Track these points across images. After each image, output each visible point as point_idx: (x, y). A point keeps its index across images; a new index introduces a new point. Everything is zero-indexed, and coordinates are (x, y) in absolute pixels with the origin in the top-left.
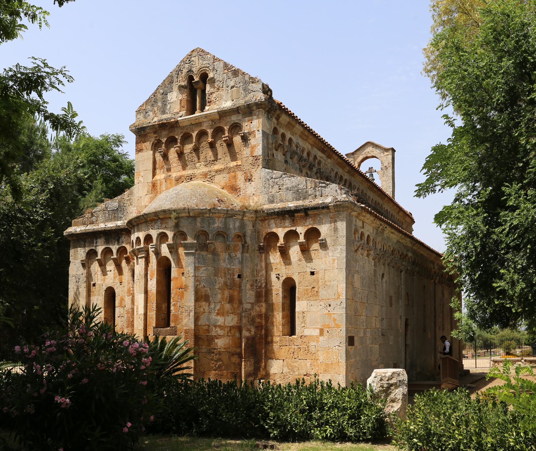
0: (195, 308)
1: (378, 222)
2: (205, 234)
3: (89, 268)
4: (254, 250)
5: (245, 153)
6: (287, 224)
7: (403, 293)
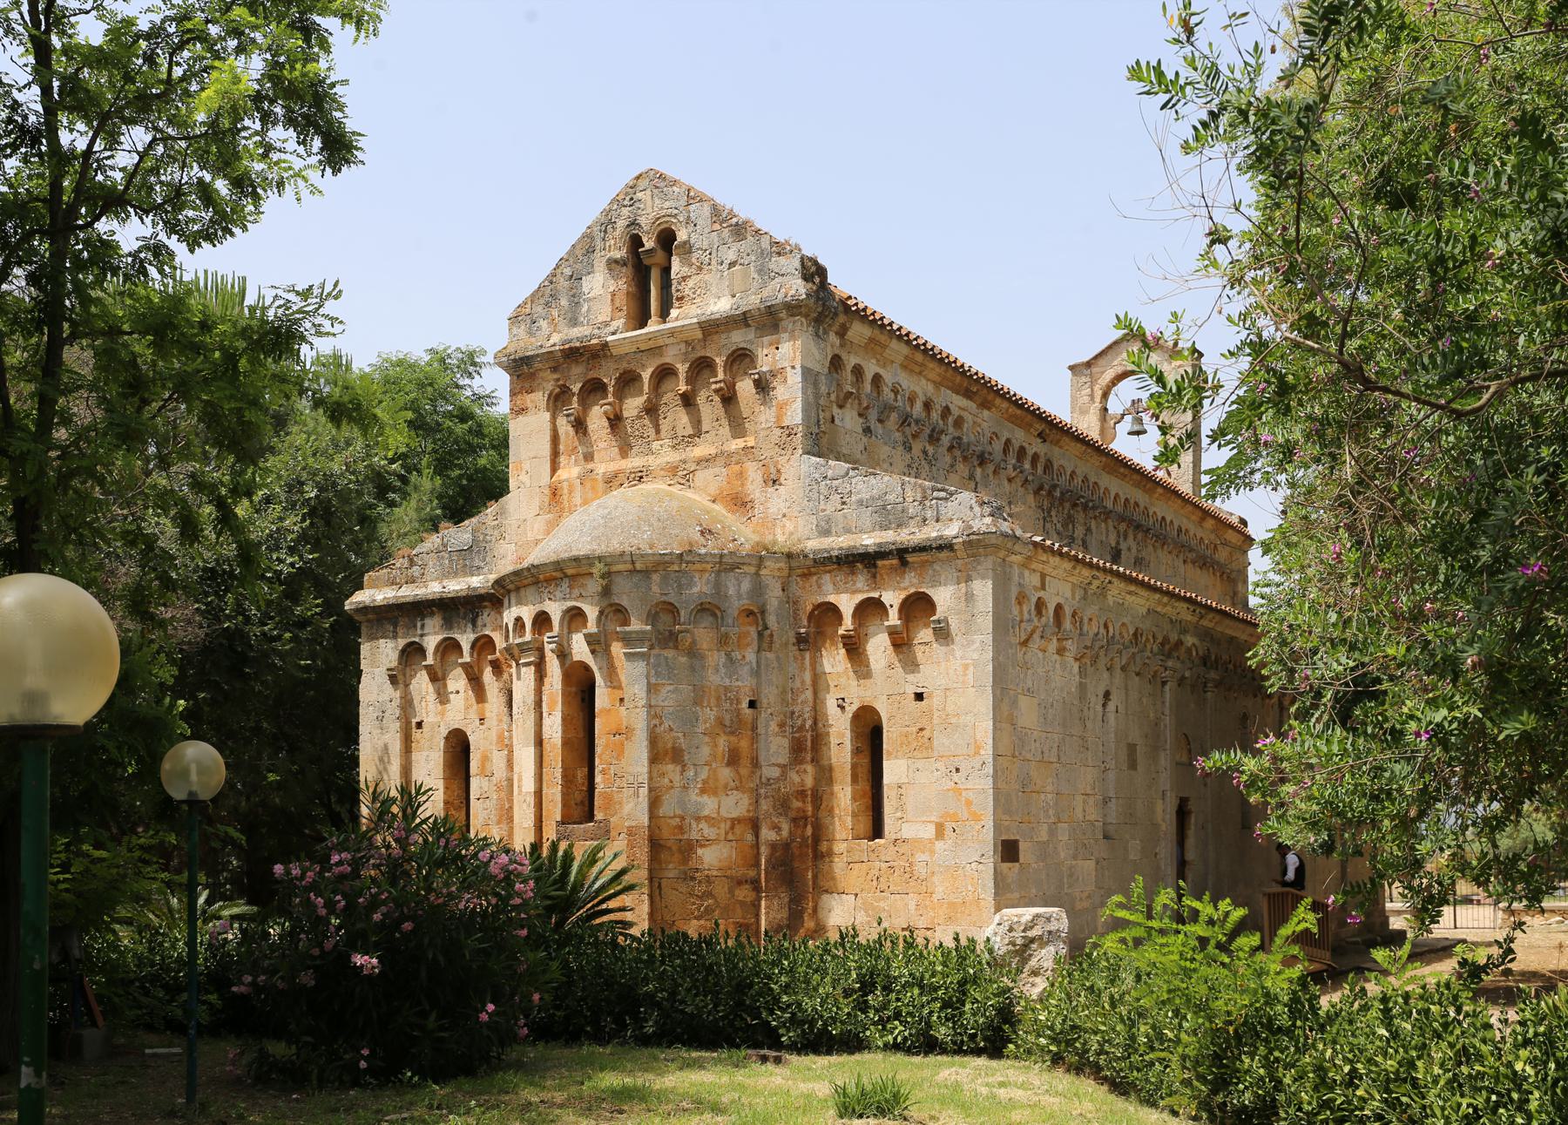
0: (650, 779)
1: (1086, 572)
2: (672, 609)
3: (407, 685)
4: (786, 644)
5: (762, 418)
6: (859, 585)
7: (1169, 736)
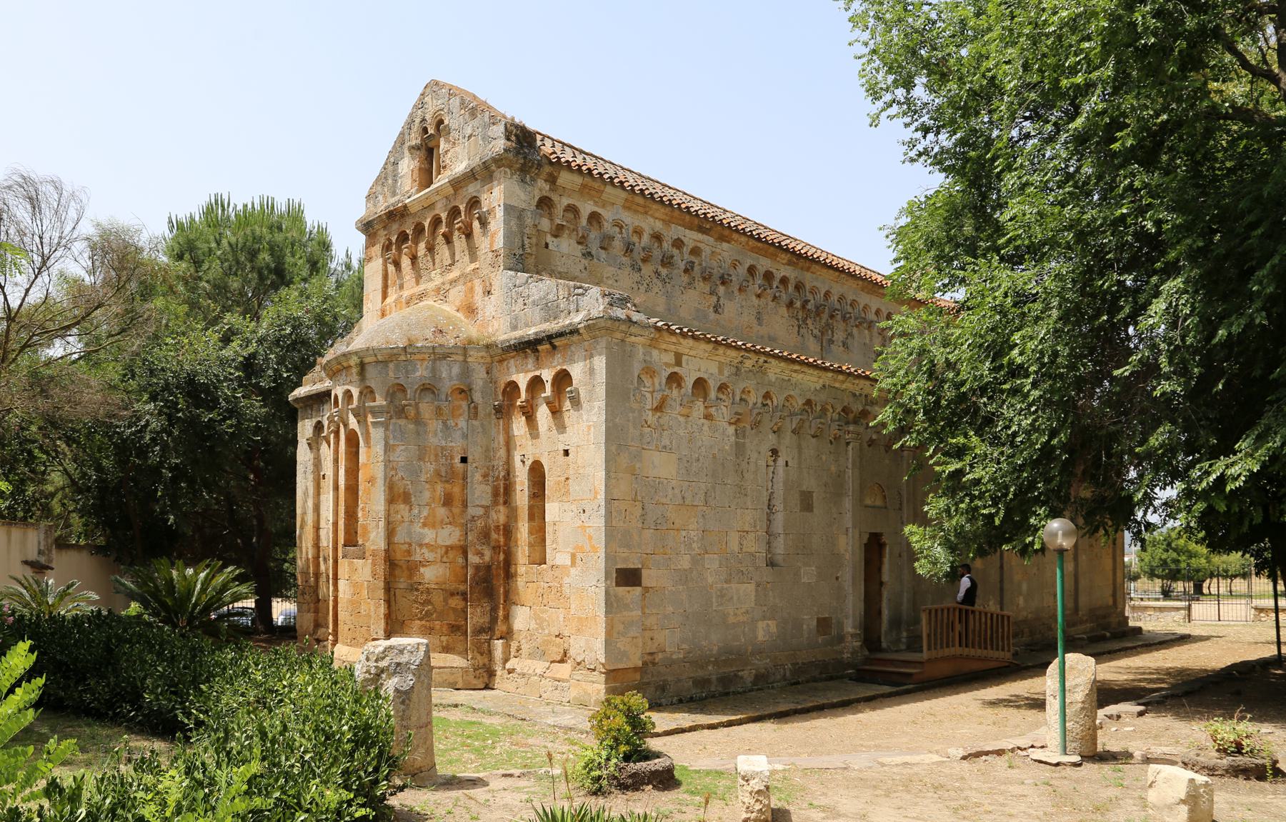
1: (732, 353)
2: (402, 389)
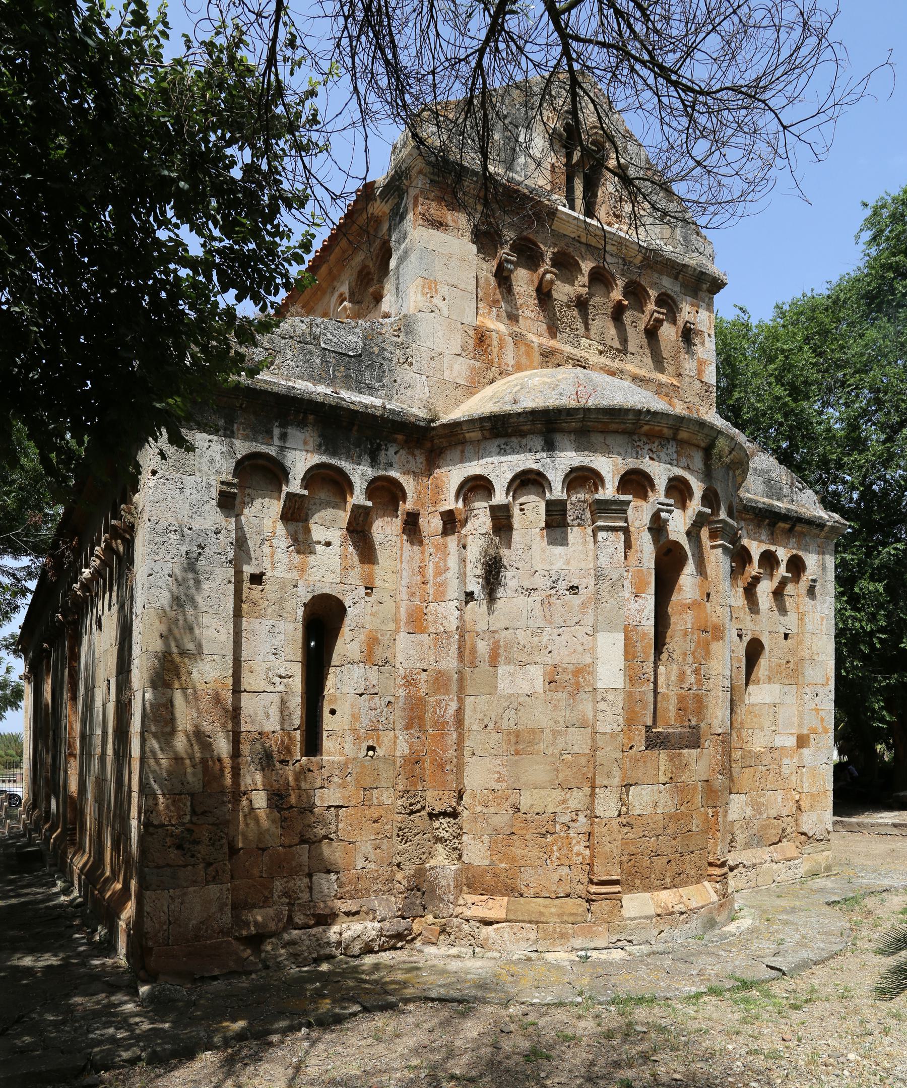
6: (763, 538)
